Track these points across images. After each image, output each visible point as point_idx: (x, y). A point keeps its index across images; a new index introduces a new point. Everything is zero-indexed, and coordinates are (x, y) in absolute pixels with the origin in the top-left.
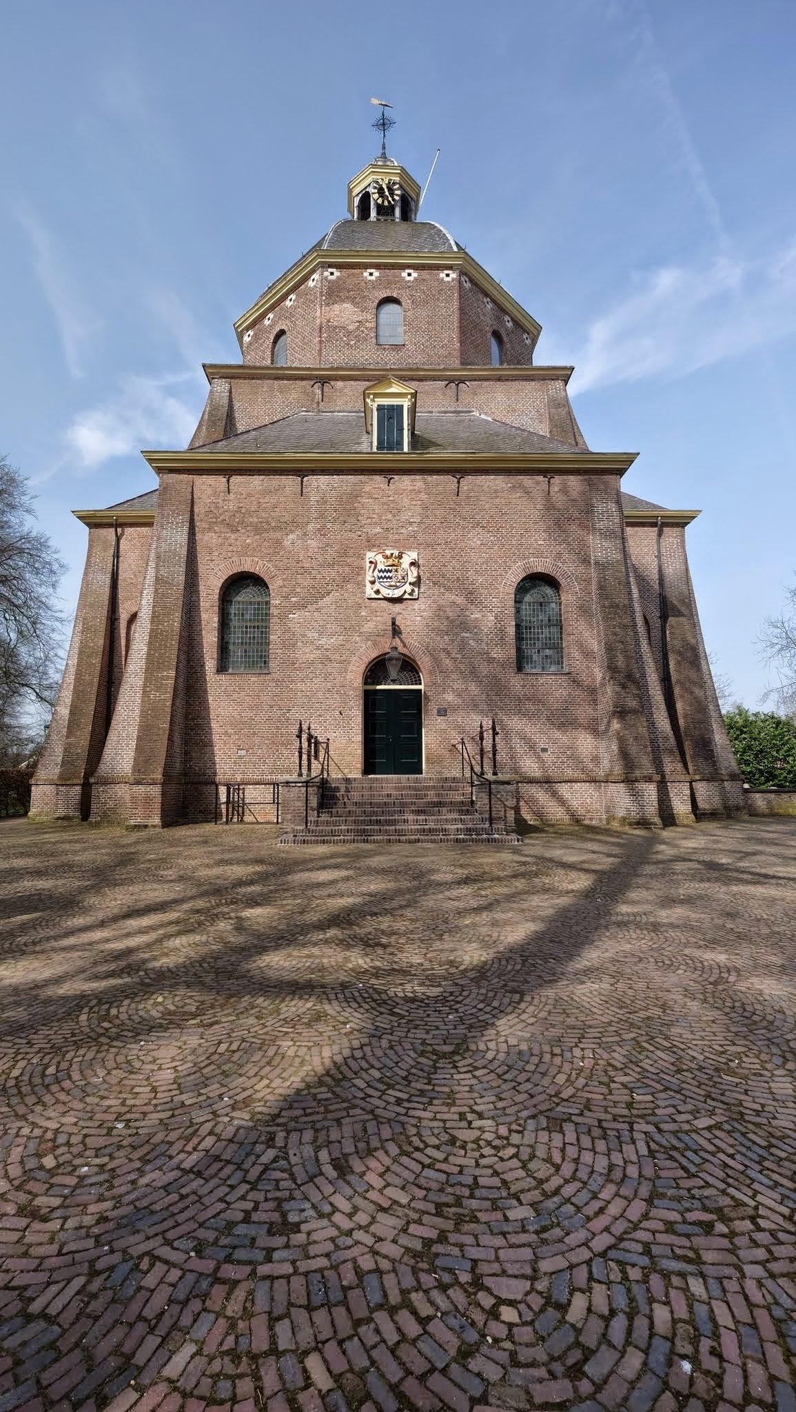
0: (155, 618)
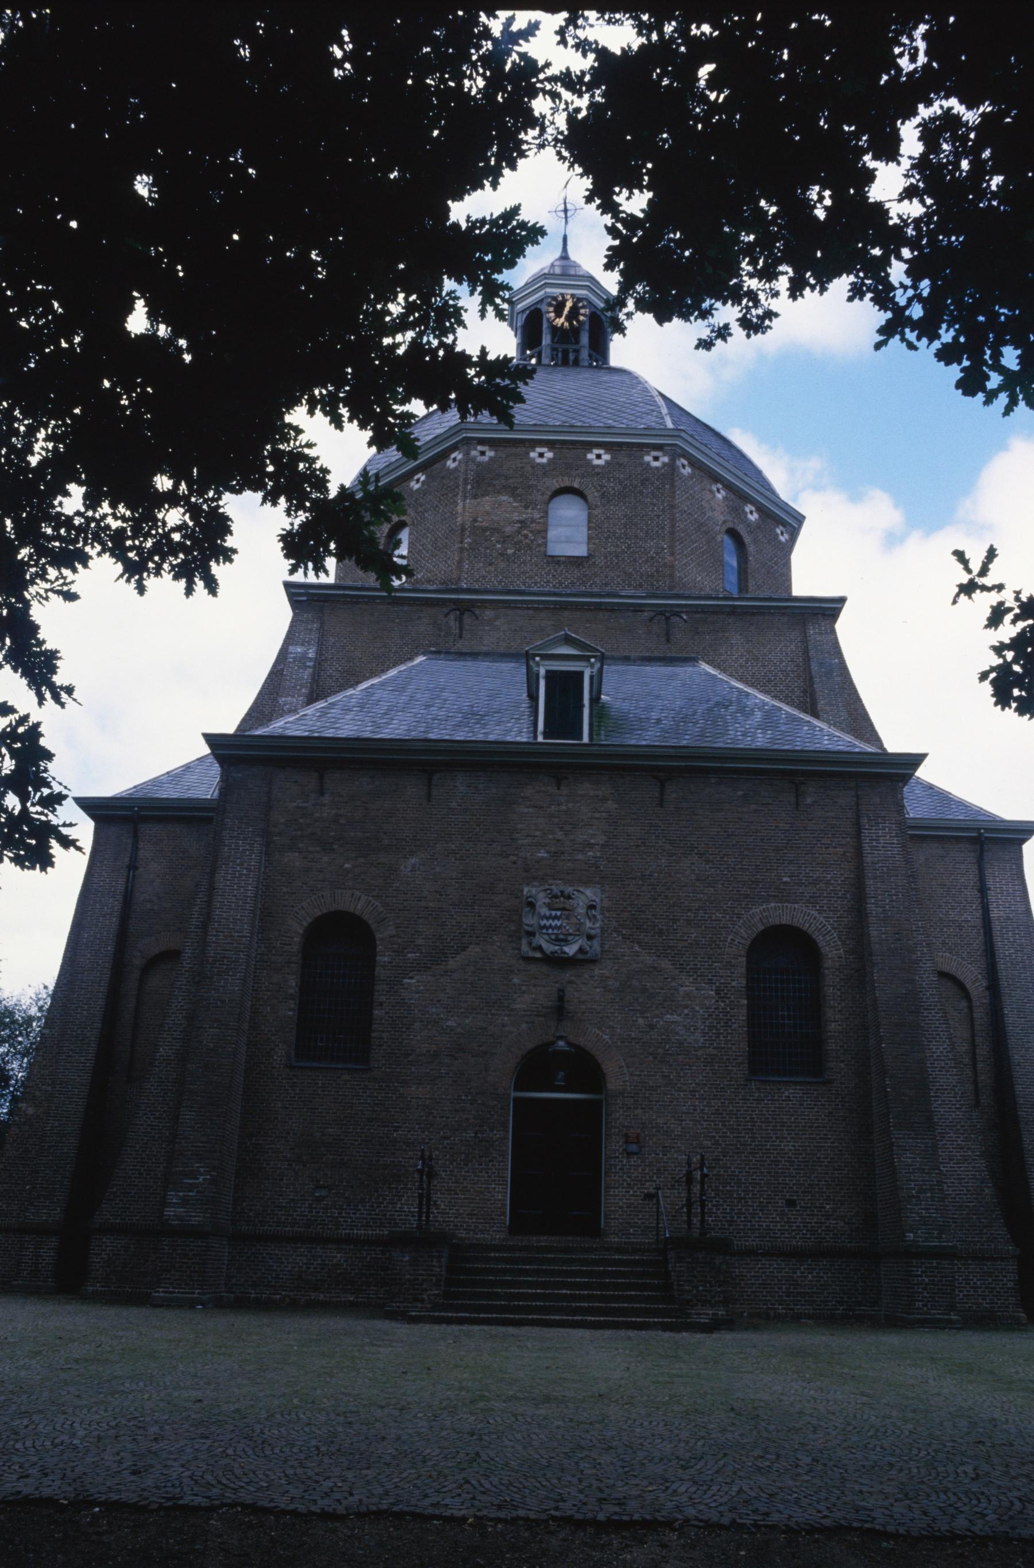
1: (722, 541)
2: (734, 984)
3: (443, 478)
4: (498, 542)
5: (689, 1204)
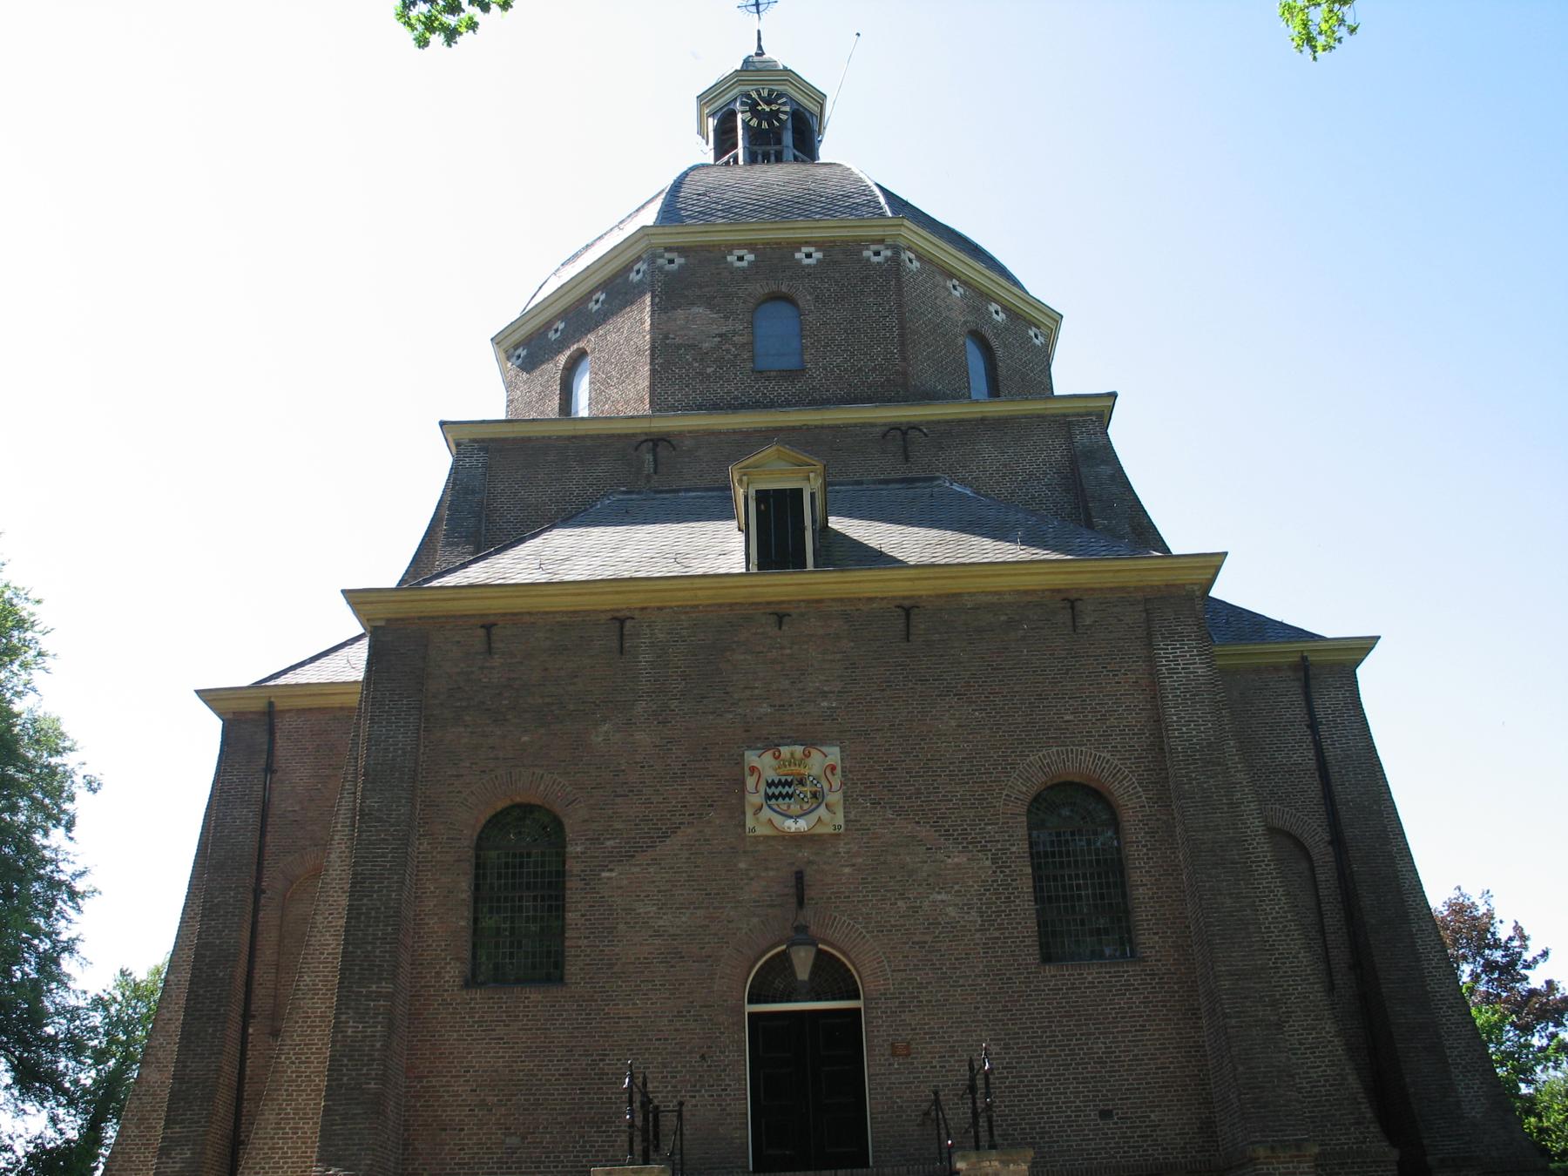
0: (358, 886)
2: (1014, 849)
5: (975, 1115)
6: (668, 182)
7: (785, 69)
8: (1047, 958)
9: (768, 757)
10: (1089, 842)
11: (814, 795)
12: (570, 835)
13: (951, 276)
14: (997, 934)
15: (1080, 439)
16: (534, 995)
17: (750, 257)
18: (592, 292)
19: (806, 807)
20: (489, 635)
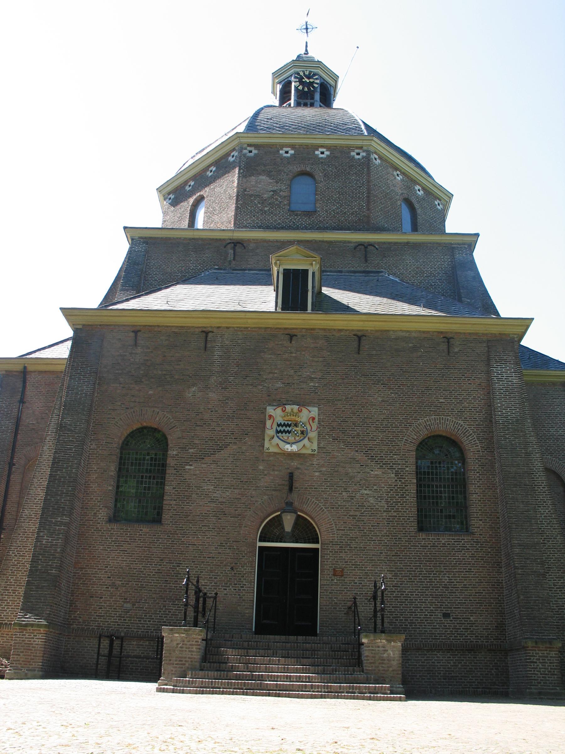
0: (56, 464)
1: (401, 205)
2: (407, 469)
3: (226, 167)
4: (259, 203)
5: (375, 611)
6: (251, 114)
7: (318, 61)
8: (421, 529)
9: (279, 410)
10: (448, 468)
11: (302, 432)
12: (170, 445)
13: (396, 169)
14: (395, 514)
15: (458, 256)
16: (145, 529)
17: (292, 152)
18: (209, 166)
19: (297, 438)
20: (136, 337)
